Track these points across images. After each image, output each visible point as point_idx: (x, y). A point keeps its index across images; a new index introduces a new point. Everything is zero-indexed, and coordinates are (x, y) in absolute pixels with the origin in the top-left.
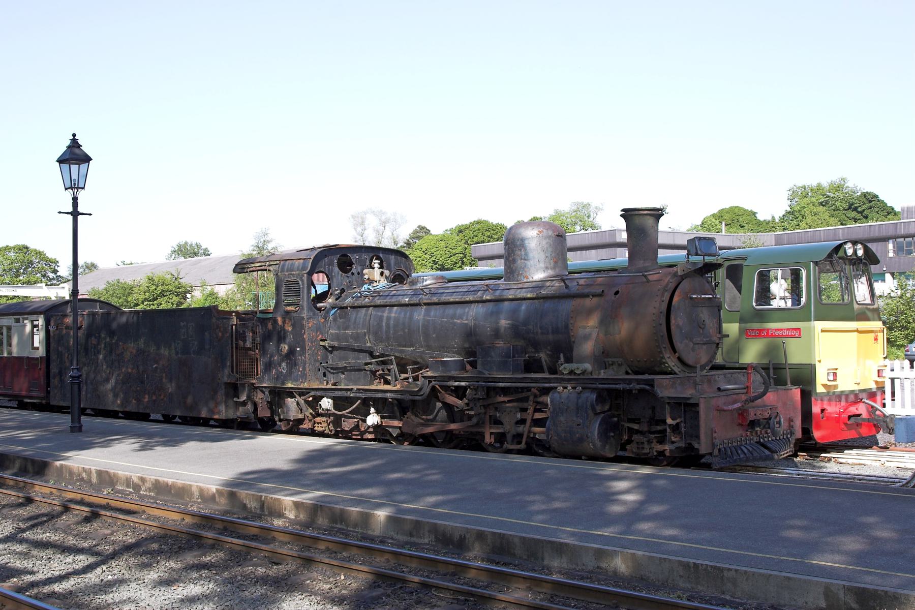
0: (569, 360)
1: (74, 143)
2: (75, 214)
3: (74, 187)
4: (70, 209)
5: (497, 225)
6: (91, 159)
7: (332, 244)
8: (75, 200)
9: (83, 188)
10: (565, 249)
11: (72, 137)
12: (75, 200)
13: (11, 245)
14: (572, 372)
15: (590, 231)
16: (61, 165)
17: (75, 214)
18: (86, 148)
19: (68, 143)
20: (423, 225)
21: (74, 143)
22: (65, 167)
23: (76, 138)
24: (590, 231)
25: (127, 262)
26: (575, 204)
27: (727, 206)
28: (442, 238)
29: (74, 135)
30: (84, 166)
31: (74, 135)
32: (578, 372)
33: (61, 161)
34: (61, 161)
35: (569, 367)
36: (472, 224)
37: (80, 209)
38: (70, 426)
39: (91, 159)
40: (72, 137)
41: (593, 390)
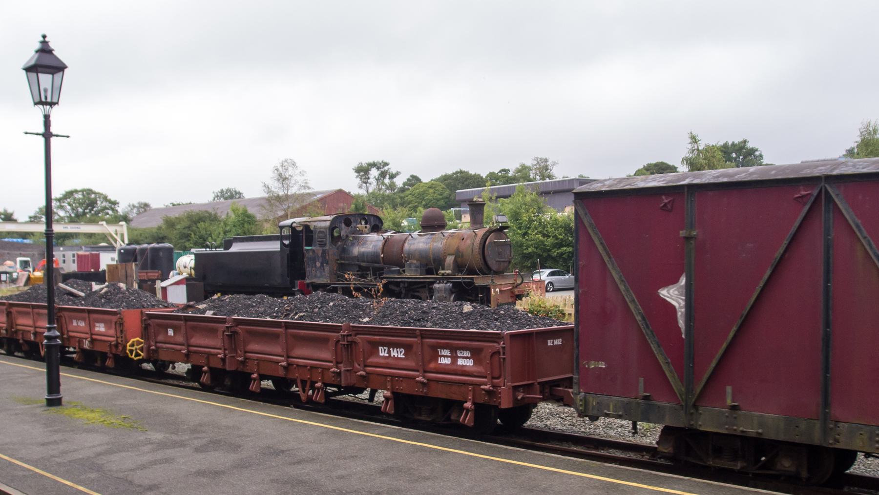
0: (443, 269)
1: (45, 49)
2: (47, 135)
3: (46, 102)
4: (53, 140)
5: (475, 175)
6: (66, 67)
7: (472, 172)
8: (47, 119)
9: (57, 103)
10: (225, 202)
11: (42, 39)
12: (47, 119)
13: (79, 189)
14: (443, 275)
15: (548, 180)
16: (28, 73)
17: (47, 135)
18: (60, 53)
19: (38, 46)
20: (415, 174)
21: (45, 49)
22: (33, 75)
23: (47, 39)
24: (548, 180)
25: (175, 203)
26: (536, 159)
27: (654, 162)
28: (431, 186)
29: (44, 37)
30: (58, 76)
31: (44, 37)
32: (445, 274)
33: (29, 69)
34: (29, 69)
35: (443, 272)
36: (454, 174)
37: (53, 130)
38: (47, 399)
39: (66, 67)
40: (42, 39)
41: (451, 282)
